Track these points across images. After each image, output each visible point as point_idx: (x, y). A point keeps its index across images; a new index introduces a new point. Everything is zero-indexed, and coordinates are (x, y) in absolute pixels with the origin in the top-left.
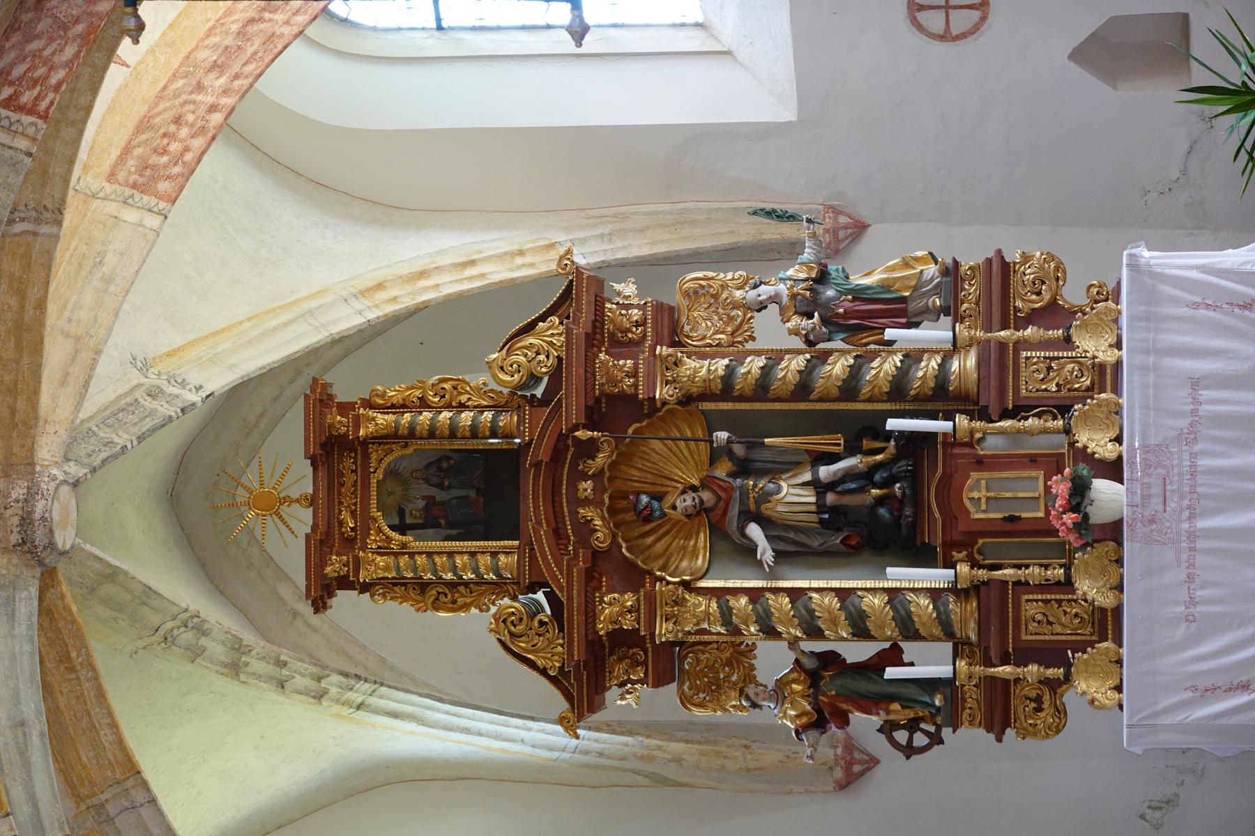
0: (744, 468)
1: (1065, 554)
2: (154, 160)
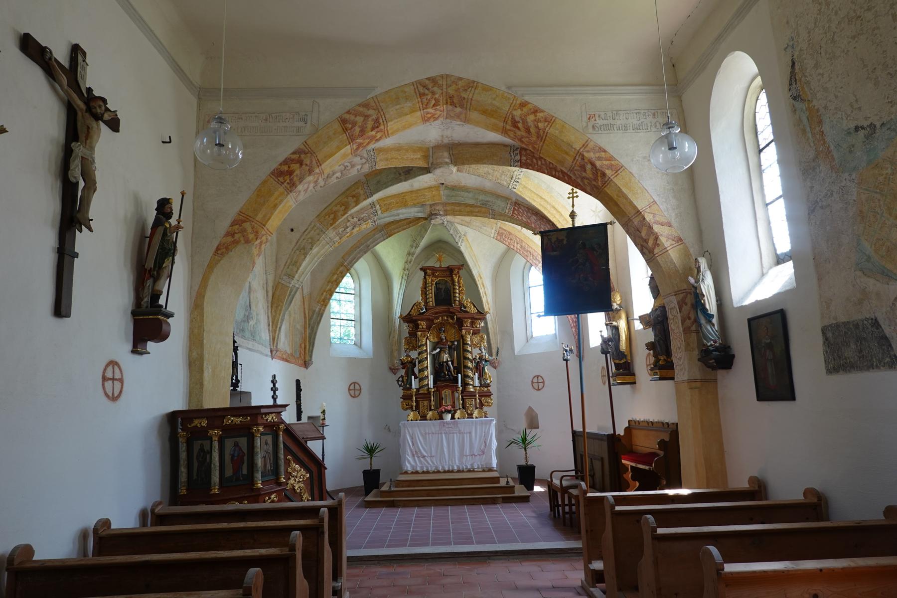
0: (450, 348)
1: (436, 408)
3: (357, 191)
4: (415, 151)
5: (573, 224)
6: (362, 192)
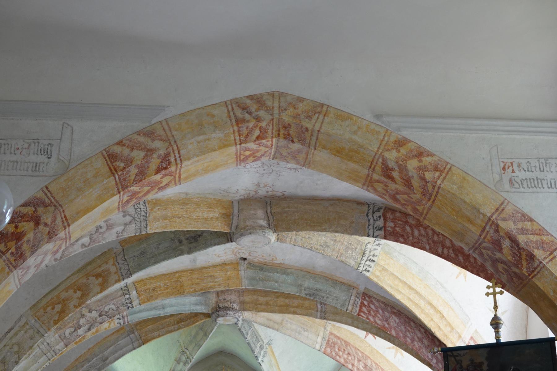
2: (337, 347)
3: (104, 267)
4: (210, 206)
5: (498, 338)
6: (113, 269)
